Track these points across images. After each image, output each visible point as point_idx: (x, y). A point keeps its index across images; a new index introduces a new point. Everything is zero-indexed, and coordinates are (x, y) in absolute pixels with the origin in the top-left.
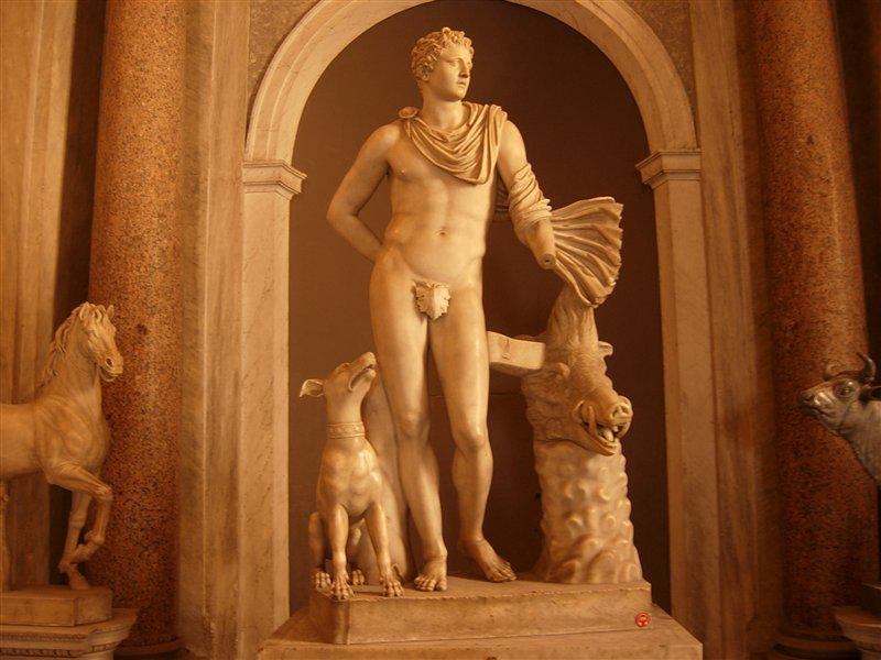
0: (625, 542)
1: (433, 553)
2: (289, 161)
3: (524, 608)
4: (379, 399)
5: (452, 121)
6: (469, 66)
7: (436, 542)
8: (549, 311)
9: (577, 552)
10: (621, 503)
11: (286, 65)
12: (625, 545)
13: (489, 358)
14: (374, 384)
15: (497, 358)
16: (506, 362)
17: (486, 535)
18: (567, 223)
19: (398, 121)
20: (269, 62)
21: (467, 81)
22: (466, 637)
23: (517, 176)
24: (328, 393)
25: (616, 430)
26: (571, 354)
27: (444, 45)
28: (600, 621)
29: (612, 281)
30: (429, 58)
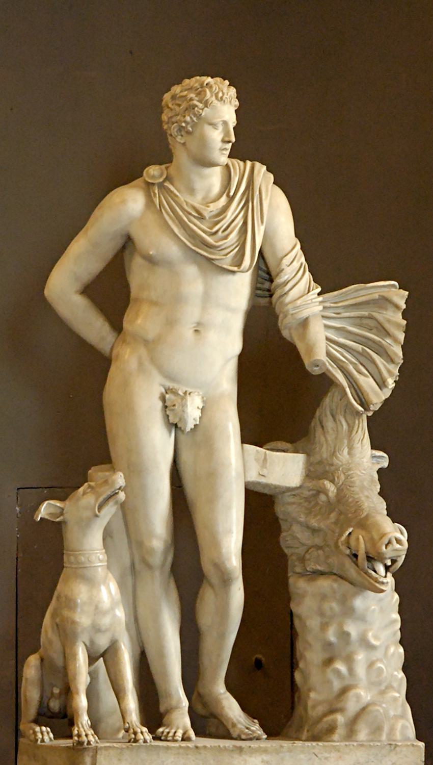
0: (397, 695)
1: (174, 703)
4: (119, 526)
5: (209, 191)
9: (339, 705)
10: (392, 650)
13: (245, 479)
15: (253, 477)
16: (263, 480)
17: (229, 688)
23: (286, 261)
24: (67, 516)
25: (389, 563)
26: (338, 469)
27: (206, 104)
29: (391, 383)
30: (188, 119)
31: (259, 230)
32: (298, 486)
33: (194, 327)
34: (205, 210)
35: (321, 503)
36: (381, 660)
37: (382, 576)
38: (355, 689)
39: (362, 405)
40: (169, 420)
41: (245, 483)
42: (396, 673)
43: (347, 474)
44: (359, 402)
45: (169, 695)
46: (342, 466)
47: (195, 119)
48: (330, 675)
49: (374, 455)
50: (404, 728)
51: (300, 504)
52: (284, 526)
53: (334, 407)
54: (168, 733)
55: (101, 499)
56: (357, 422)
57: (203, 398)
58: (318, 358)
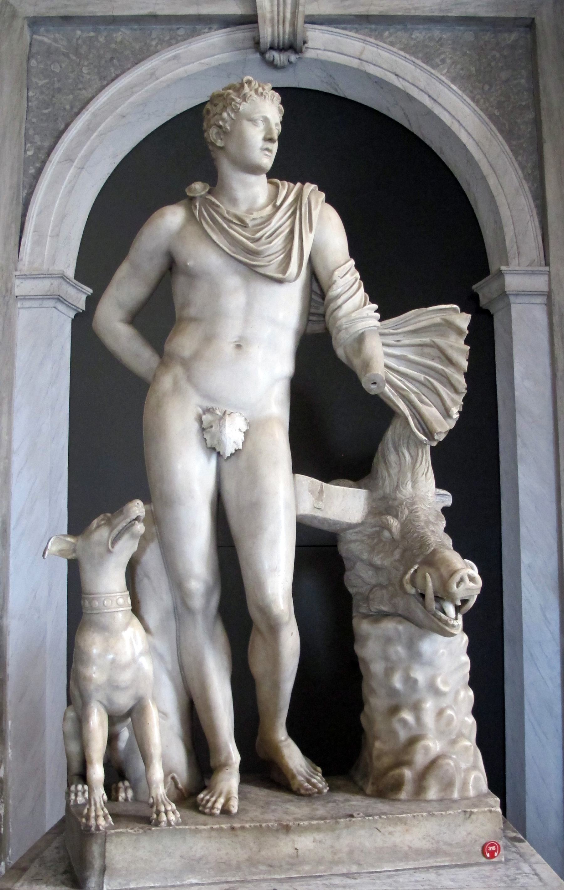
0: (468, 743)
1: (223, 758)
2: (71, 273)
3: (338, 837)
6: (277, 130)
7: (227, 746)
8: (375, 450)
9: (406, 758)
10: (462, 694)
11: (69, 159)
12: (466, 748)
13: (297, 506)
14: (144, 540)
16: (319, 514)
17: (292, 732)
18: (397, 338)
19: (185, 201)
20: (48, 155)
21: (275, 147)
22: (262, 876)
23: (337, 273)
26: (401, 504)
27: (245, 98)
28: (436, 853)
29: (456, 416)
31: (307, 237)
32: (360, 521)
33: (235, 342)
34: (246, 216)
35: (384, 539)
36: (450, 707)
37: (452, 618)
38: (423, 740)
39: (425, 434)
40: (206, 444)
41: (297, 517)
42: (466, 719)
43: (410, 508)
44: (422, 431)
45: (218, 750)
46: (406, 499)
47: (232, 115)
48: (398, 727)
49: (438, 493)
50: (477, 779)
51: (362, 541)
52: (347, 564)
53: (397, 440)
54: (208, 801)
55: (115, 532)
56: (420, 454)
57: (246, 419)
58: (377, 373)
